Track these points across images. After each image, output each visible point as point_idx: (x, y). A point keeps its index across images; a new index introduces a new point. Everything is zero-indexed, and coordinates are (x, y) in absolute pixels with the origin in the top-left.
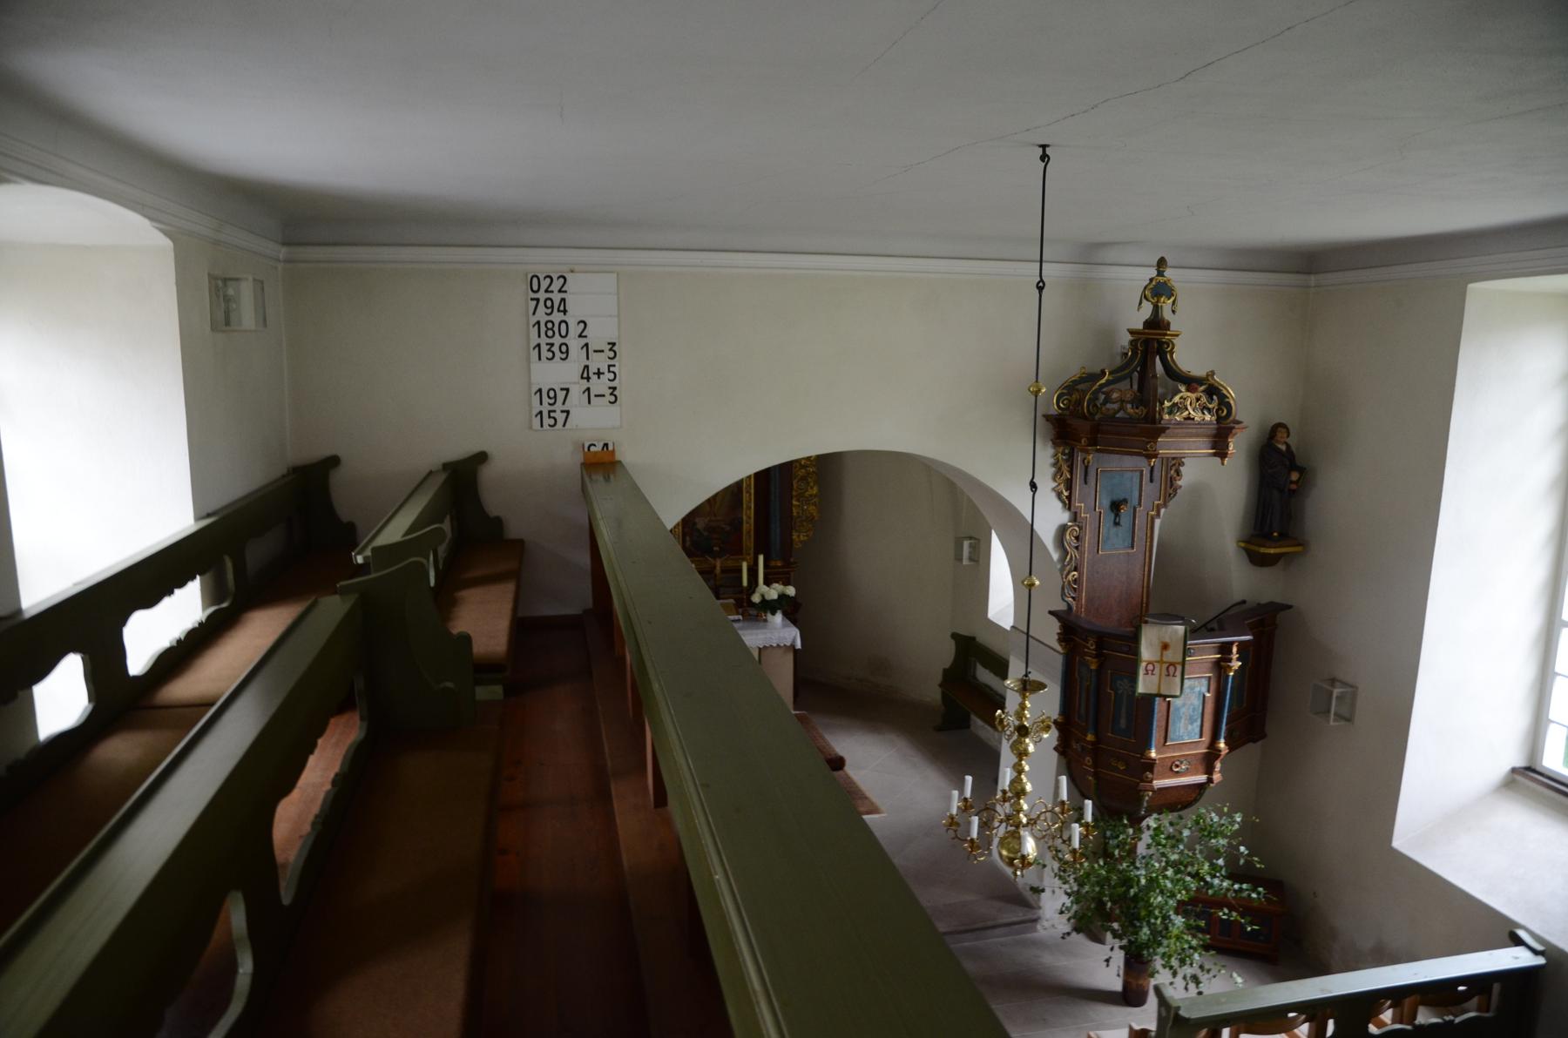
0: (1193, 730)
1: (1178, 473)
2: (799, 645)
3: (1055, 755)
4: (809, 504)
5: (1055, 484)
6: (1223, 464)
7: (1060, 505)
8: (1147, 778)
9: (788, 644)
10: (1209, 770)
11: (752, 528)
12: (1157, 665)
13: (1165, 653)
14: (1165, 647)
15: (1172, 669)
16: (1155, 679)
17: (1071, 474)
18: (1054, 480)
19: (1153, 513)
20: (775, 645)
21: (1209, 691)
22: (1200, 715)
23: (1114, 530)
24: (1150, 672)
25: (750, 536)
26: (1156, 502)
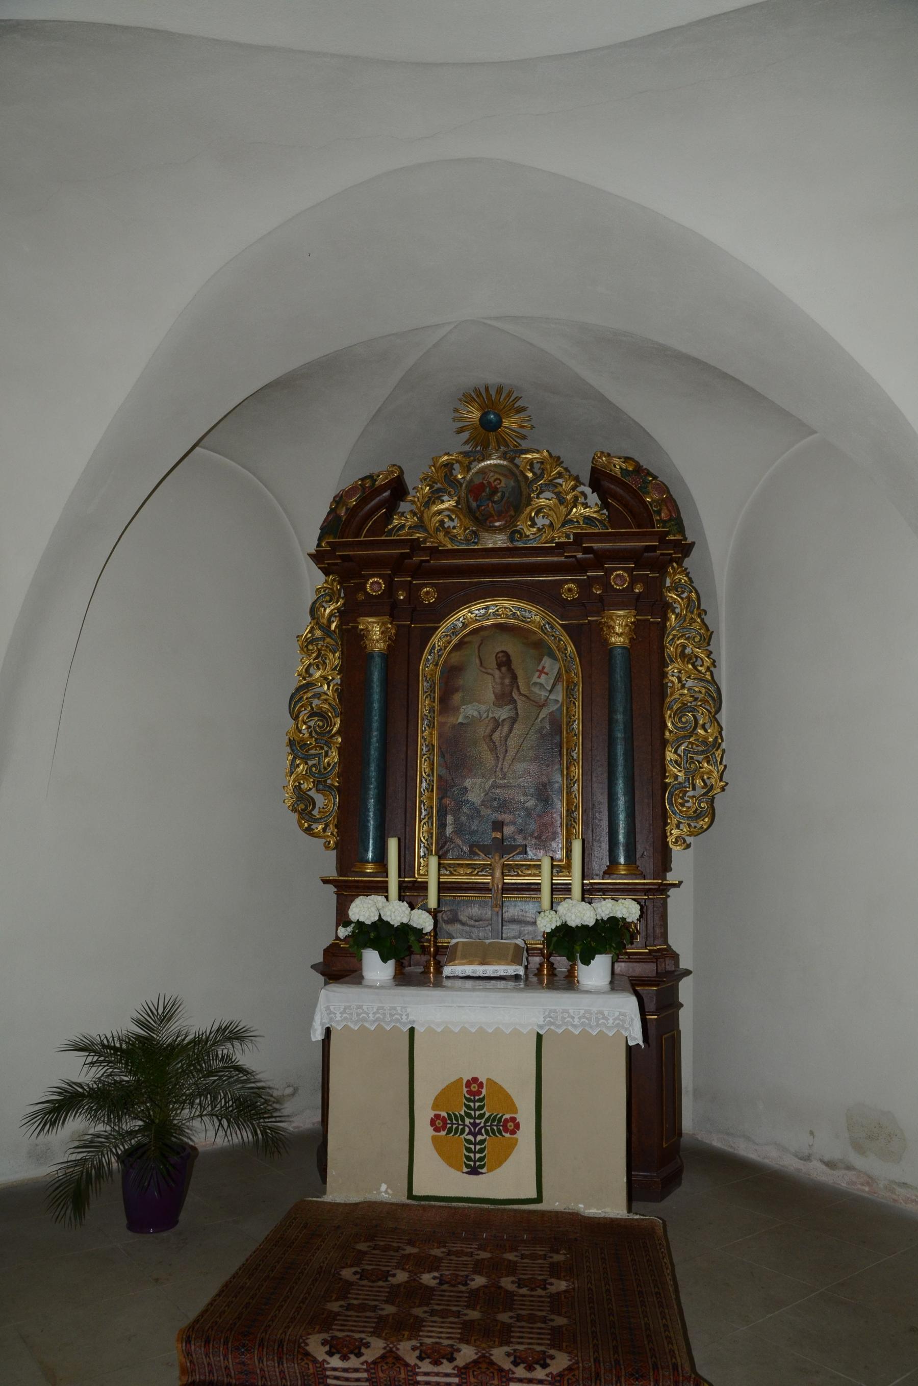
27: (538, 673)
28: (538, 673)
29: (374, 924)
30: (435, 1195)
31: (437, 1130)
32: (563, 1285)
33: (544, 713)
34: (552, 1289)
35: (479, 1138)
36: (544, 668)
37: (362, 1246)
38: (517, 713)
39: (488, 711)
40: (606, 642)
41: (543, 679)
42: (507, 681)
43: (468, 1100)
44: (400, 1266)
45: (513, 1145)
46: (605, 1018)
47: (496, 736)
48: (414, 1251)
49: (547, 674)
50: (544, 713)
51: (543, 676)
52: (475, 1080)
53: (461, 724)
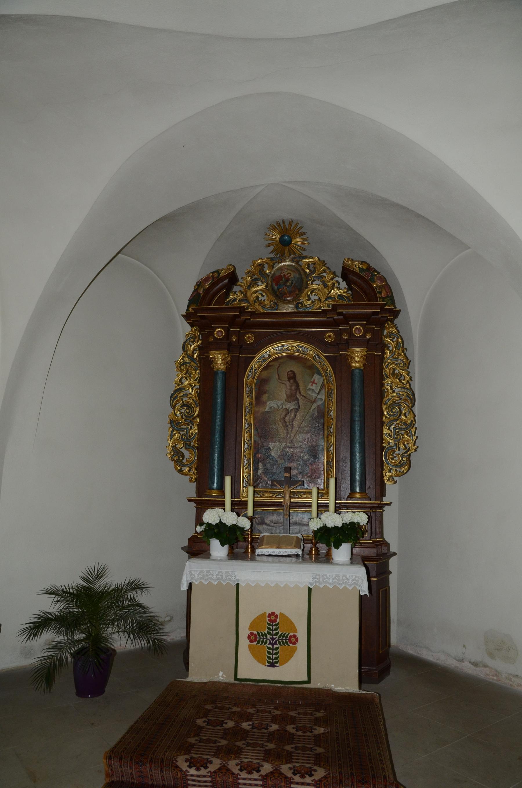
29: (217, 524)
31: (251, 641)
32: (321, 730)
33: (314, 406)
34: (316, 732)
35: (275, 646)
37: (208, 707)
38: (299, 406)
39: (282, 405)
40: (350, 366)
42: (294, 388)
43: (269, 625)
44: (230, 718)
45: (294, 650)
47: (287, 419)
48: (238, 709)
50: (314, 406)
51: (314, 385)
52: (273, 613)
53: (267, 412)
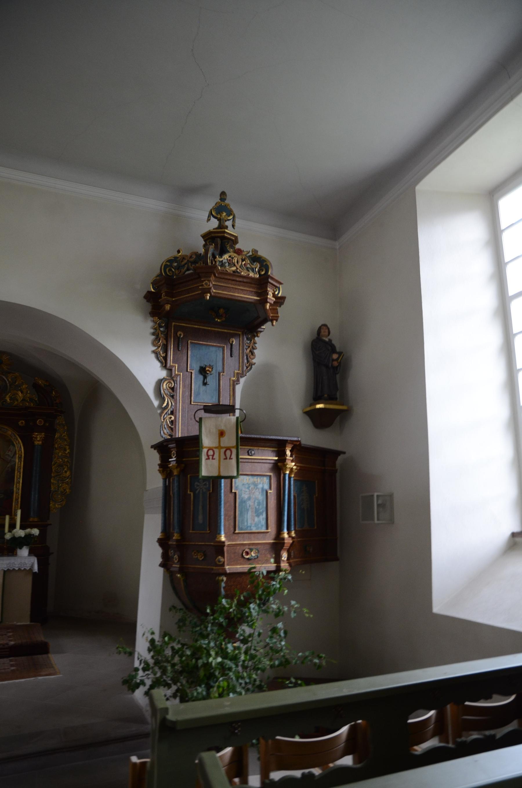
0: (260, 522)
1: (252, 353)
2: (36, 569)
3: (161, 570)
4: (63, 483)
5: (154, 348)
6: (273, 325)
7: (158, 364)
8: (219, 561)
9: (28, 569)
10: (278, 560)
11: (20, 496)
12: (216, 451)
13: (221, 439)
14: (222, 434)
15: (228, 452)
16: (215, 462)
17: (167, 341)
18: (154, 345)
19: (234, 379)
20: (17, 569)
21: (270, 488)
22: (265, 509)
23: (203, 388)
24: (211, 457)
25: (18, 502)
26: (236, 371)
27: (8, 451)
28: (8, 451)
30: (519, 291)
36: (10, 449)
41: (9, 453)
46: (26, 564)
49: (11, 451)
